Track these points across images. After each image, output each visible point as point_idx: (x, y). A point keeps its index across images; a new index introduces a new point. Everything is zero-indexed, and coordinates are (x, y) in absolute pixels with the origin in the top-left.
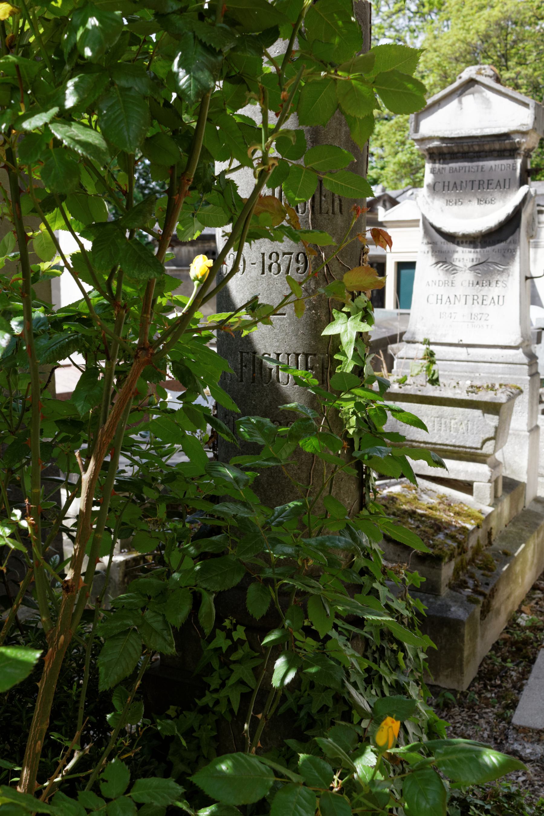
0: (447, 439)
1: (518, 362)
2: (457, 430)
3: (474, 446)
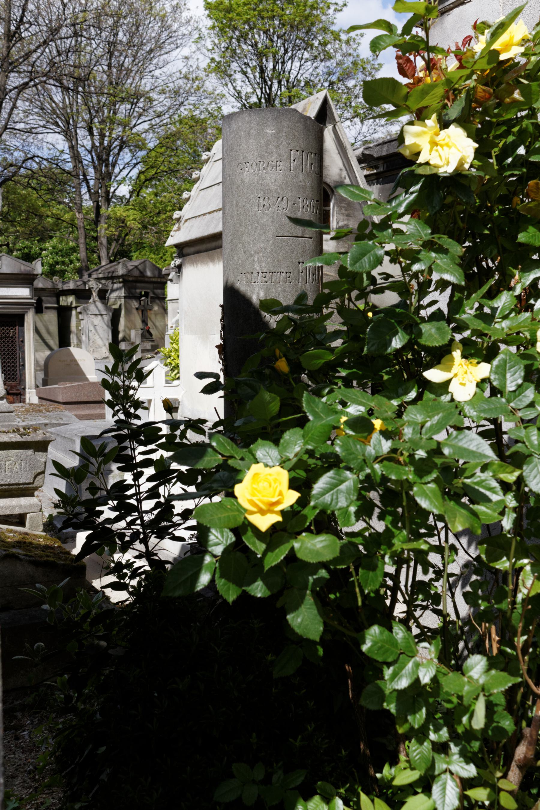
0: (2, 480)
1: (6, 410)
2: (11, 470)
3: (27, 481)
